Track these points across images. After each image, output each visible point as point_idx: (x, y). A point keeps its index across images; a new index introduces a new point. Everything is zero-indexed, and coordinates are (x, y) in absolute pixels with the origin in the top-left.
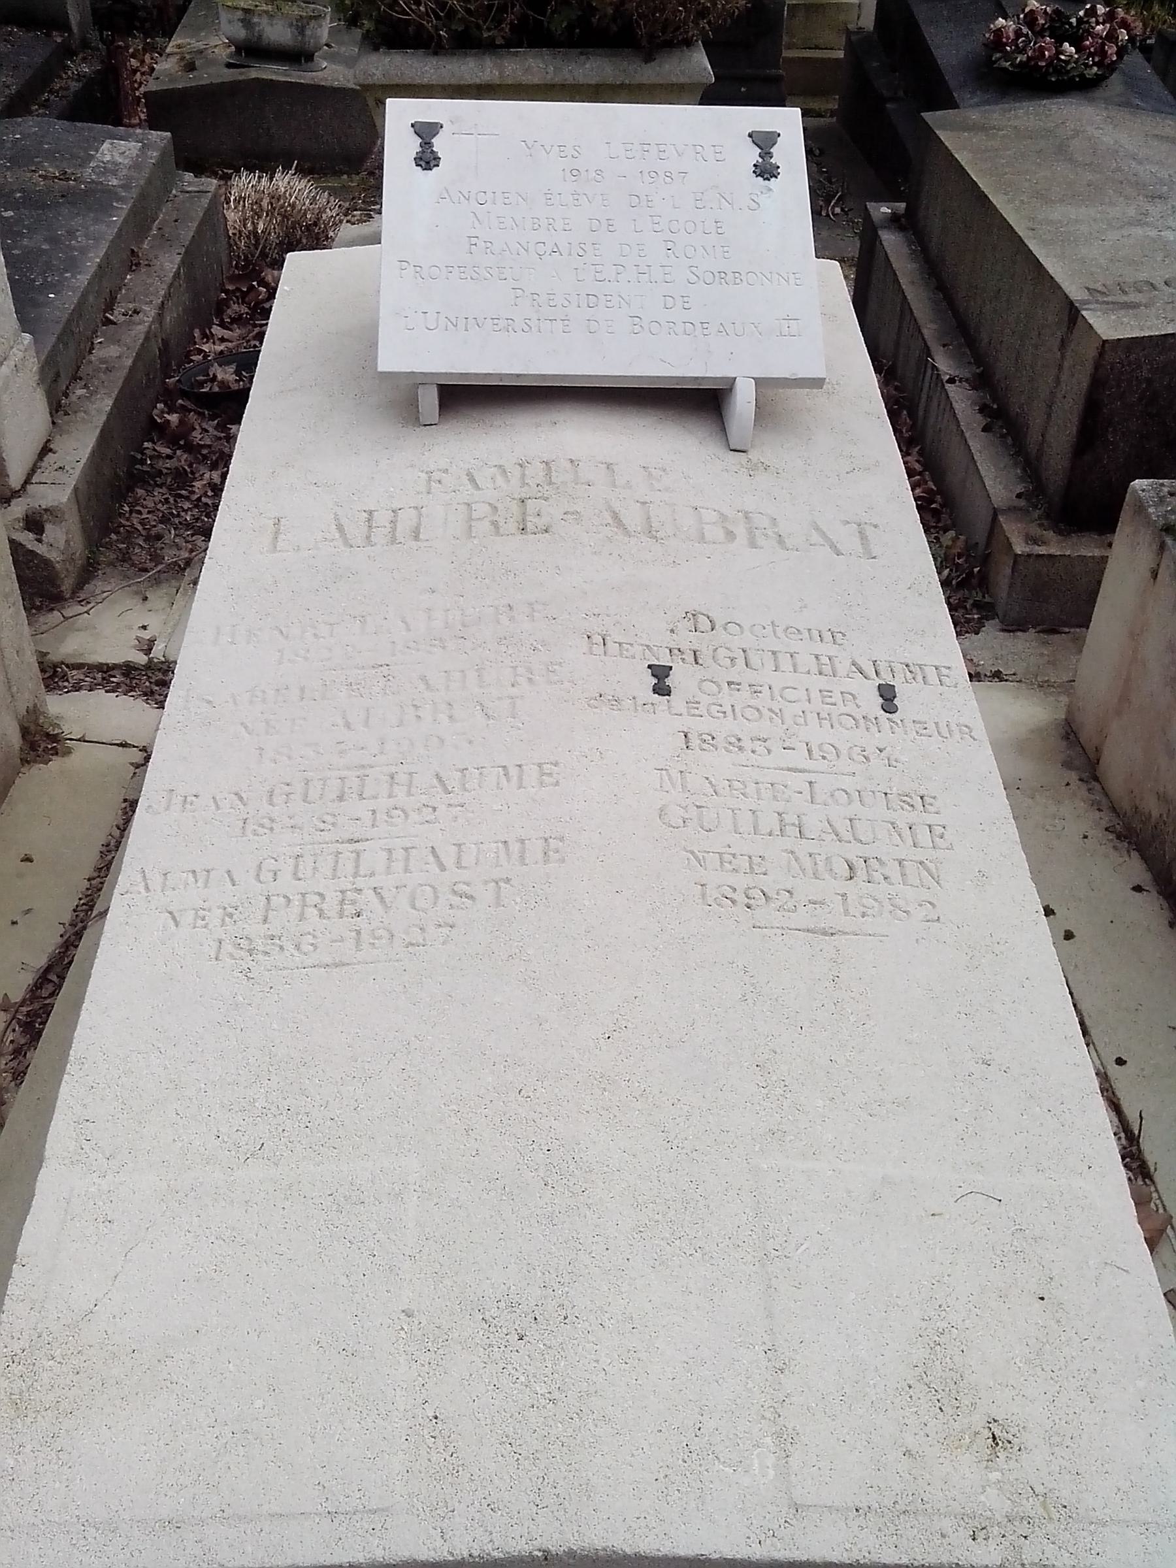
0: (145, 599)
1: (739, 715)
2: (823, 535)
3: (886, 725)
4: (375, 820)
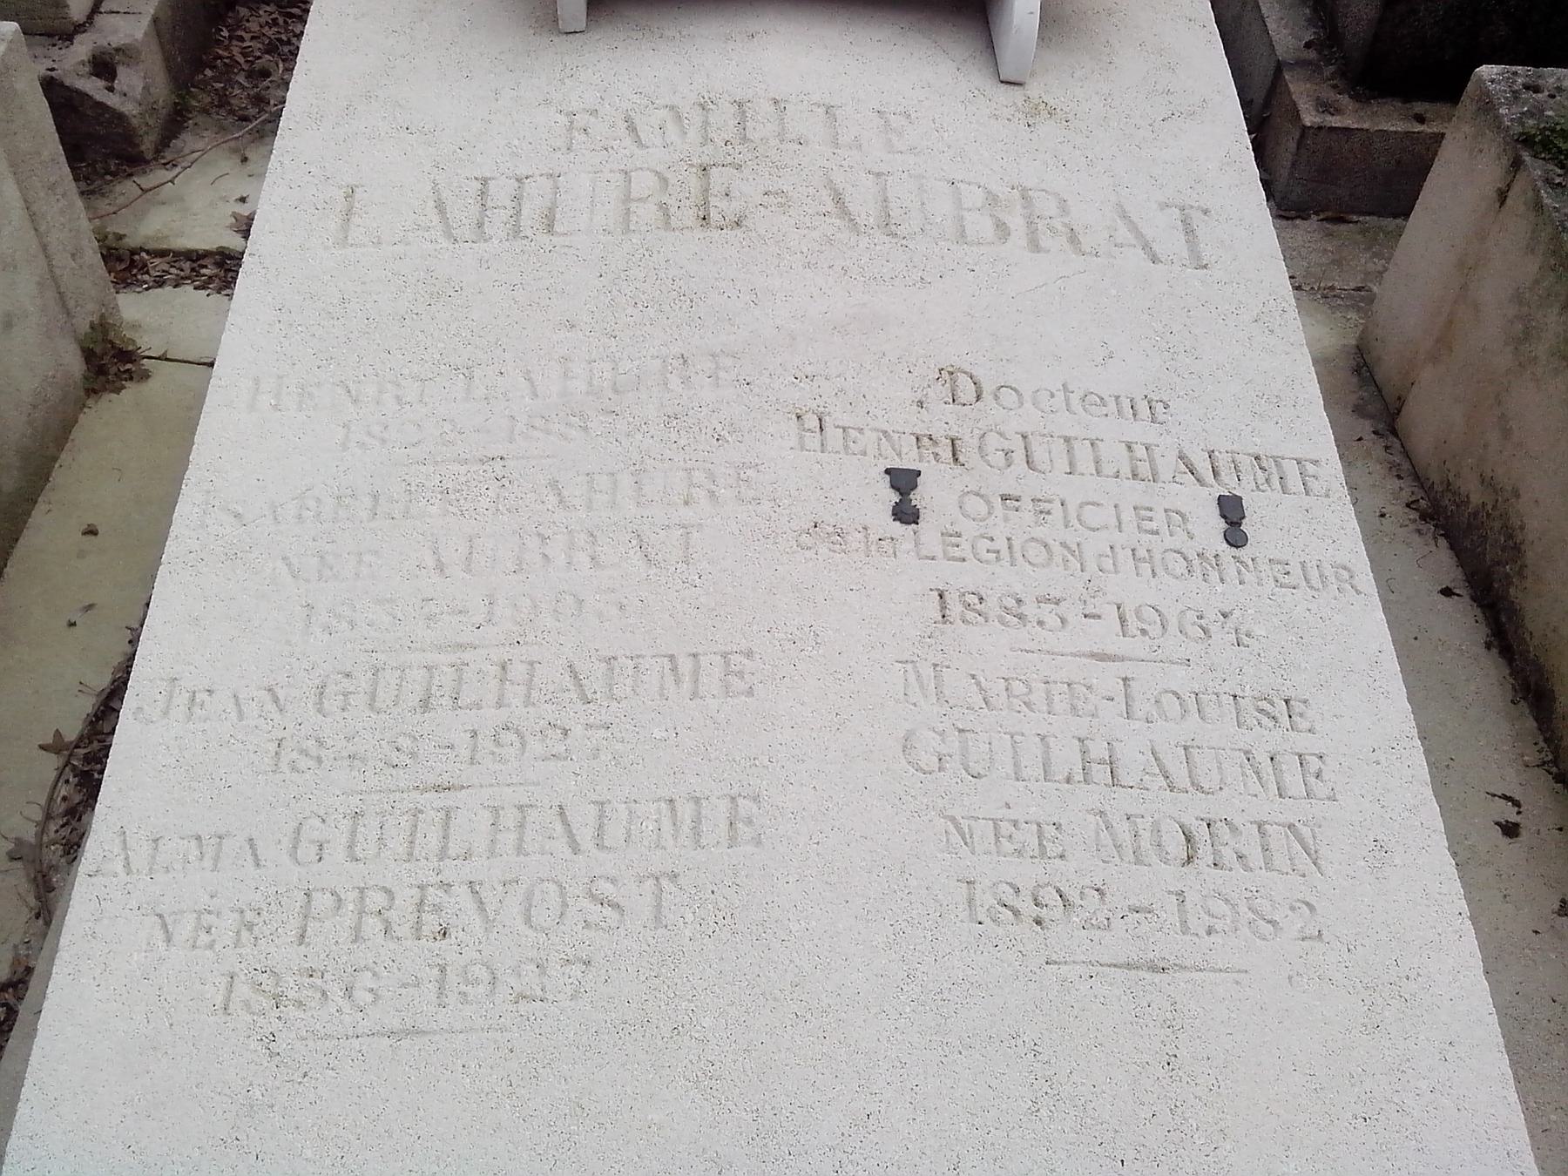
0: (245, 160)
1: (1018, 555)
2: (1134, 228)
3: (1231, 569)
4: (474, 749)
